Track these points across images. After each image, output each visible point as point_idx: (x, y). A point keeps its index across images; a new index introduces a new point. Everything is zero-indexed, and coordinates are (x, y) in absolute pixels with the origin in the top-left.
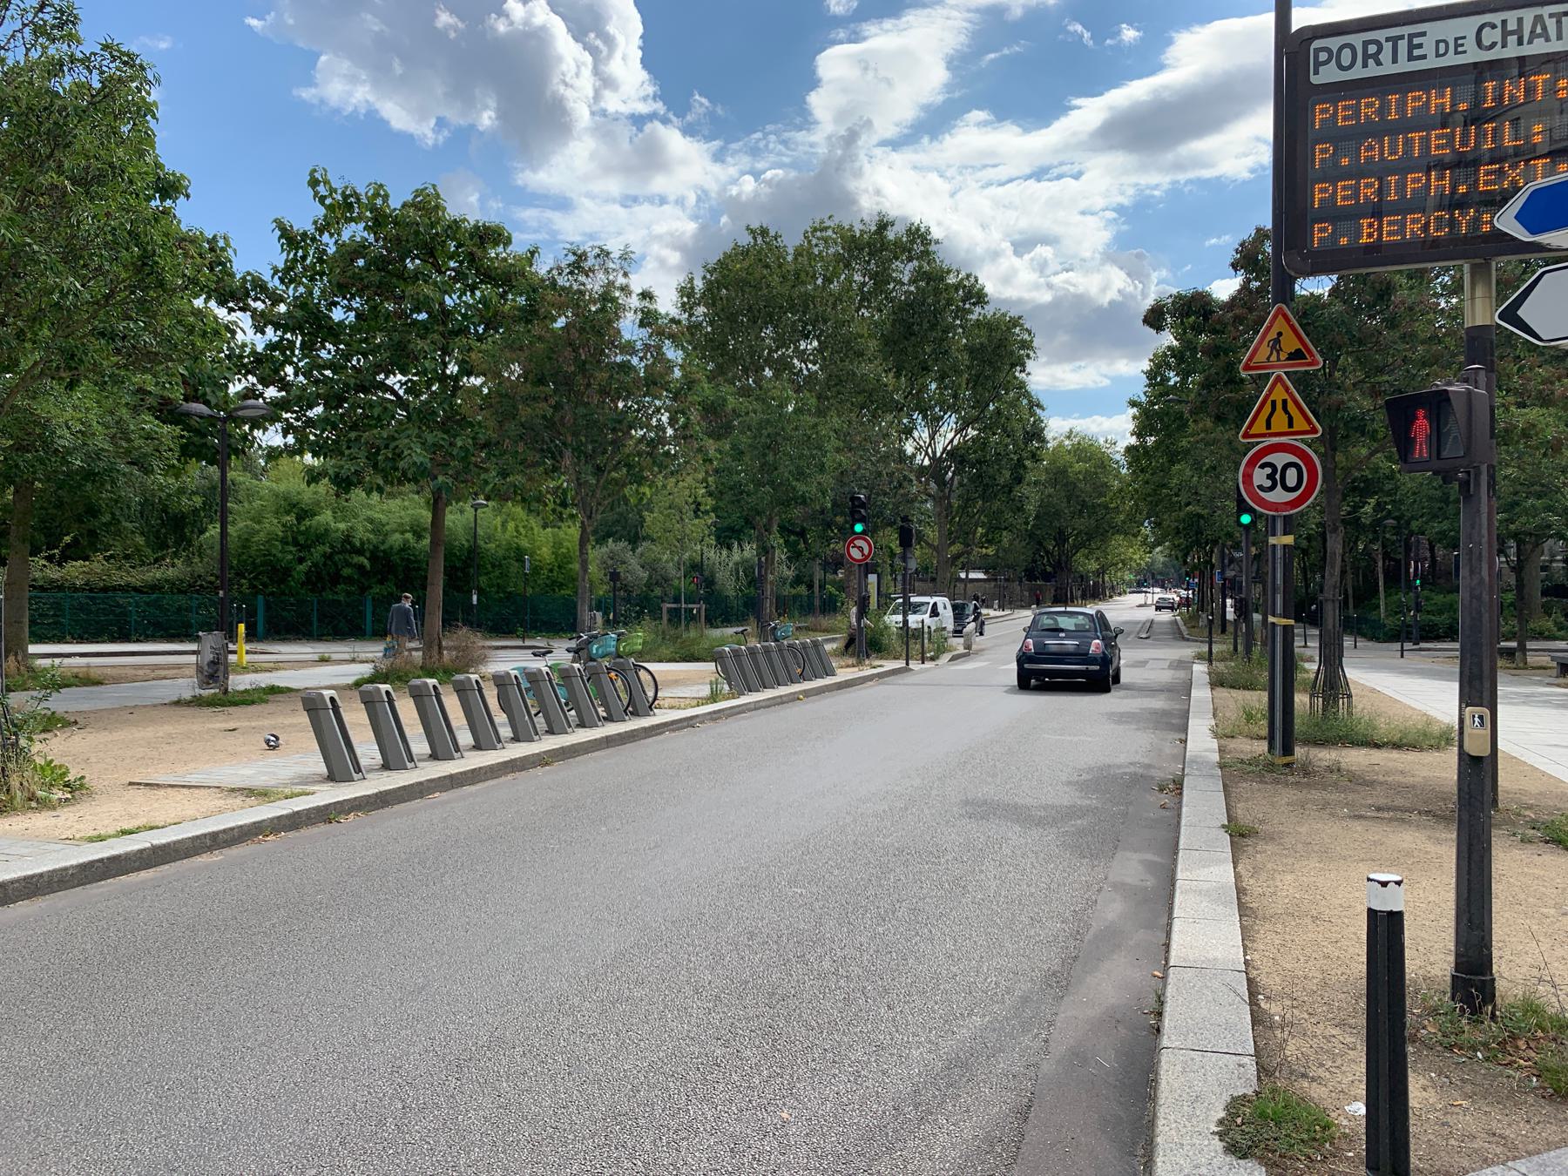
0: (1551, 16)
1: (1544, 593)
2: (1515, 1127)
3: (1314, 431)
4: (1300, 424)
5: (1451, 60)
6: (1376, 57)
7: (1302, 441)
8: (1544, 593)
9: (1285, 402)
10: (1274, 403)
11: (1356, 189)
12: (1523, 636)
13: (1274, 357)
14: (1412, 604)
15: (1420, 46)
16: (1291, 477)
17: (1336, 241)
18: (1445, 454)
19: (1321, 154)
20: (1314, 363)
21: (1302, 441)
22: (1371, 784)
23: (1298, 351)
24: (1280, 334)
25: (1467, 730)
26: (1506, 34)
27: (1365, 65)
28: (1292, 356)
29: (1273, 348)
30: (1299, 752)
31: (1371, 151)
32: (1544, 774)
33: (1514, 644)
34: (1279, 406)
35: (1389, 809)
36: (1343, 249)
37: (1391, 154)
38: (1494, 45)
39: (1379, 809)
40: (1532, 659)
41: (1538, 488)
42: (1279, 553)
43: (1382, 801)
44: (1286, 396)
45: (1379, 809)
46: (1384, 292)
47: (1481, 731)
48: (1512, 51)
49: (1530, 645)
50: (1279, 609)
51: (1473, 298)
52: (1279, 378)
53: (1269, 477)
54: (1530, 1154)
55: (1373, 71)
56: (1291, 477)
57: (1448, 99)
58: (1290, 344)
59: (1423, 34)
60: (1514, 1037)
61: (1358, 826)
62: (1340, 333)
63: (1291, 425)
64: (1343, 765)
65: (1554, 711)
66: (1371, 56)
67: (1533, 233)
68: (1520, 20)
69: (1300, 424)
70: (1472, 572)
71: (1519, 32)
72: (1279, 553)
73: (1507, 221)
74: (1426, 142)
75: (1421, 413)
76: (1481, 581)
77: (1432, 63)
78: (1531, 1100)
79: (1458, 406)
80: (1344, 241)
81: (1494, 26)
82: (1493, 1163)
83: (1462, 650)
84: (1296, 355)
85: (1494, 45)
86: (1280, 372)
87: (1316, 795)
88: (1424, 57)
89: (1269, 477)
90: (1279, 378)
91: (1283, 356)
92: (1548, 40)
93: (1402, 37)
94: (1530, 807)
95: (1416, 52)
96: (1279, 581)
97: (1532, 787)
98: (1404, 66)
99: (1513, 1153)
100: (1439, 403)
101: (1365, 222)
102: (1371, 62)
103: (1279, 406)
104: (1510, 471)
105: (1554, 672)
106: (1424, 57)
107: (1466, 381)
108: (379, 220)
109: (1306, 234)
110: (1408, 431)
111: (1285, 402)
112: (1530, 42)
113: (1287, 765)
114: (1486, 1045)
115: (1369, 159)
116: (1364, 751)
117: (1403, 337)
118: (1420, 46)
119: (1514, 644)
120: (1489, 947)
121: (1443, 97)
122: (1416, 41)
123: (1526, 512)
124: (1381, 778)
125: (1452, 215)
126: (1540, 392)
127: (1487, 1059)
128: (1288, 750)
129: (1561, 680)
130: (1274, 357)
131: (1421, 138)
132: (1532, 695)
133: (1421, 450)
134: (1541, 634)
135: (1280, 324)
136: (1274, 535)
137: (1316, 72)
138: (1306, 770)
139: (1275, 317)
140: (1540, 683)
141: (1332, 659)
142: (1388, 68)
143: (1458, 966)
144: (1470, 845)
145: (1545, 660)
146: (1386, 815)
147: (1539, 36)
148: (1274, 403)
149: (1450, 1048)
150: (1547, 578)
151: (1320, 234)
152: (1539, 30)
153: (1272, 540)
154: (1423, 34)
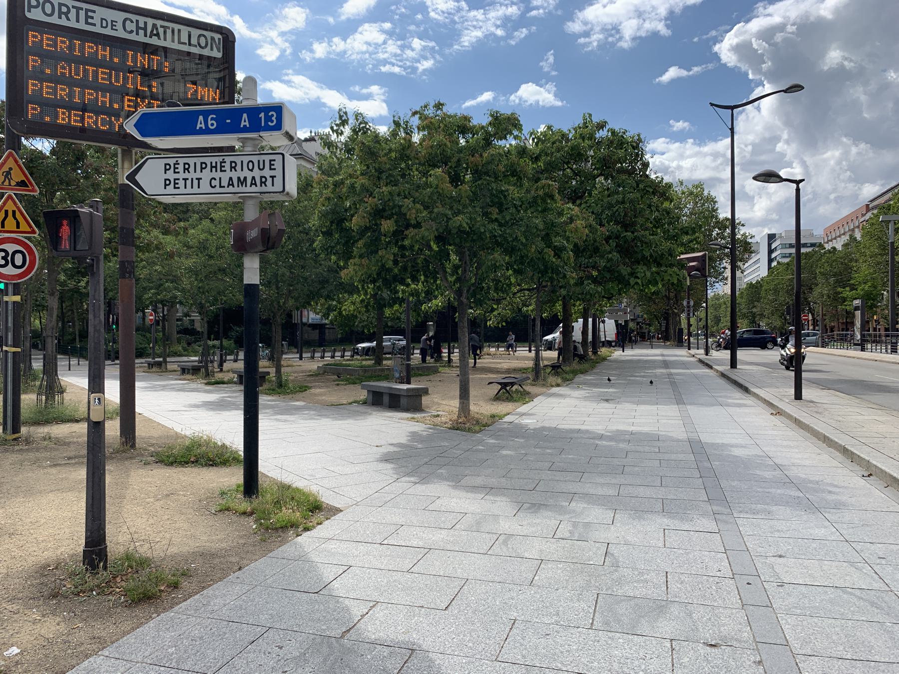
0: (162, 27)
1: (178, 333)
2: (101, 629)
3: (33, 232)
4: (24, 227)
5: (108, 32)
6: (66, 14)
7: (26, 238)
8: (178, 333)
9: (14, 212)
10: (6, 212)
11: (55, 89)
12: (165, 356)
13: (7, 183)
14: (111, 339)
15: (92, 18)
16: (19, 259)
17: (43, 118)
18: (79, 247)
19: (33, 62)
20: (34, 190)
21: (26, 238)
22: (68, 444)
23: (23, 182)
24: (11, 169)
25: (92, 407)
26: (138, 28)
27: (60, 17)
28: (18, 184)
29: (6, 177)
30: (24, 430)
31: (63, 69)
32: (163, 426)
33: (161, 359)
34: (10, 214)
35: (76, 457)
36: (46, 124)
37: (76, 75)
38: (131, 32)
39: (69, 458)
40: (169, 367)
41: (171, 278)
42: (10, 307)
43: (72, 454)
44: (15, 209)
45: (69, 458)
46: (80, 156)
47: (99, 407)
48: (141, 38)
49: (168, 359)
50: (10, 343)
51: (123, 168)
52: (10, 197)
53: (3, 258)
54: (112, 643)
55: (63, 22)
56: (19, 259)
57: (108, 53)
58: (17, 176)
59: (94, 12)
60: (114, 578)
61: (53, 471)
62: (53, 176)
63: (18, 227)
64: (52, 435)
65: (174, 393)
66: (64, 13)
67: (143, 136)
68: (145, 23)
69: (24, 227)
70: (95, 317)
71: (145, 29)
72: (10, 307)
73: (130, 128)
74: (96, 74)
75: (65, 222)
76: (100, 321)
77: (97, 29)
78: (119, 610)
79: (85, 222)
80: (47, 119)
81: (132, 22)
82: (91, 655)
83: (121, 365)
84: (22, 184)
85: (131, 32)
86: (11, 193)
87: (31, 455)
88: (94, 25)
89: (3, 258)
90: (10, 197)
91: (13, 183)
92: (159, 38)
93: (82, 9)
94: (153, 445)
95: (90, 21)
96: (10, 324)
97: (155, 433)
98: (81, 26)
99: (102, 643)
100: (74, 217)
101: (60, 110)
102: (63, 16)
103: (10, 214)
104: (157, 267)
105: (179, 373)
106: (94, 25)
107: (91, 207)
108: (506, 322)
109: (23, 111)
110: (58, 232)
111: (14, 212)
112: (151, 37)
113: (15, 439)
114: (98, 586)
115: (63, 74)
116: (68, 425)
117: (93, 185)
118: (92, 18)
119: (161, 359)
120: (104, 529)
121: (105, 51)
122: (90, 14)
123: (165, 289)
124: (75, 440)
125: (110, 119)
126: (164, 226)
127: (98, 594)
128: (16, 430)
129: (182, 377)
130: (7, 183)
131: (93, 71)
132: (167, 385)
133: (65, 245)
134: (176, 353)
135: (11, 163)
136: (7, 295)
137: (29, 11)
138: (28, 441)
139: (8, 157)
140: (172, 379)
141: (50, 370)
142: (72, 24)
143: (87, 544)
144: (93, 473)
145: (175, 367)
146: (73, 461)
147: (155, 35)
148: (6, 212)
149: (78, 594)
150: (182, 325)
151: (32, 111)
152: (155, 32)
153: (6, 298)
154: (94, 12)
